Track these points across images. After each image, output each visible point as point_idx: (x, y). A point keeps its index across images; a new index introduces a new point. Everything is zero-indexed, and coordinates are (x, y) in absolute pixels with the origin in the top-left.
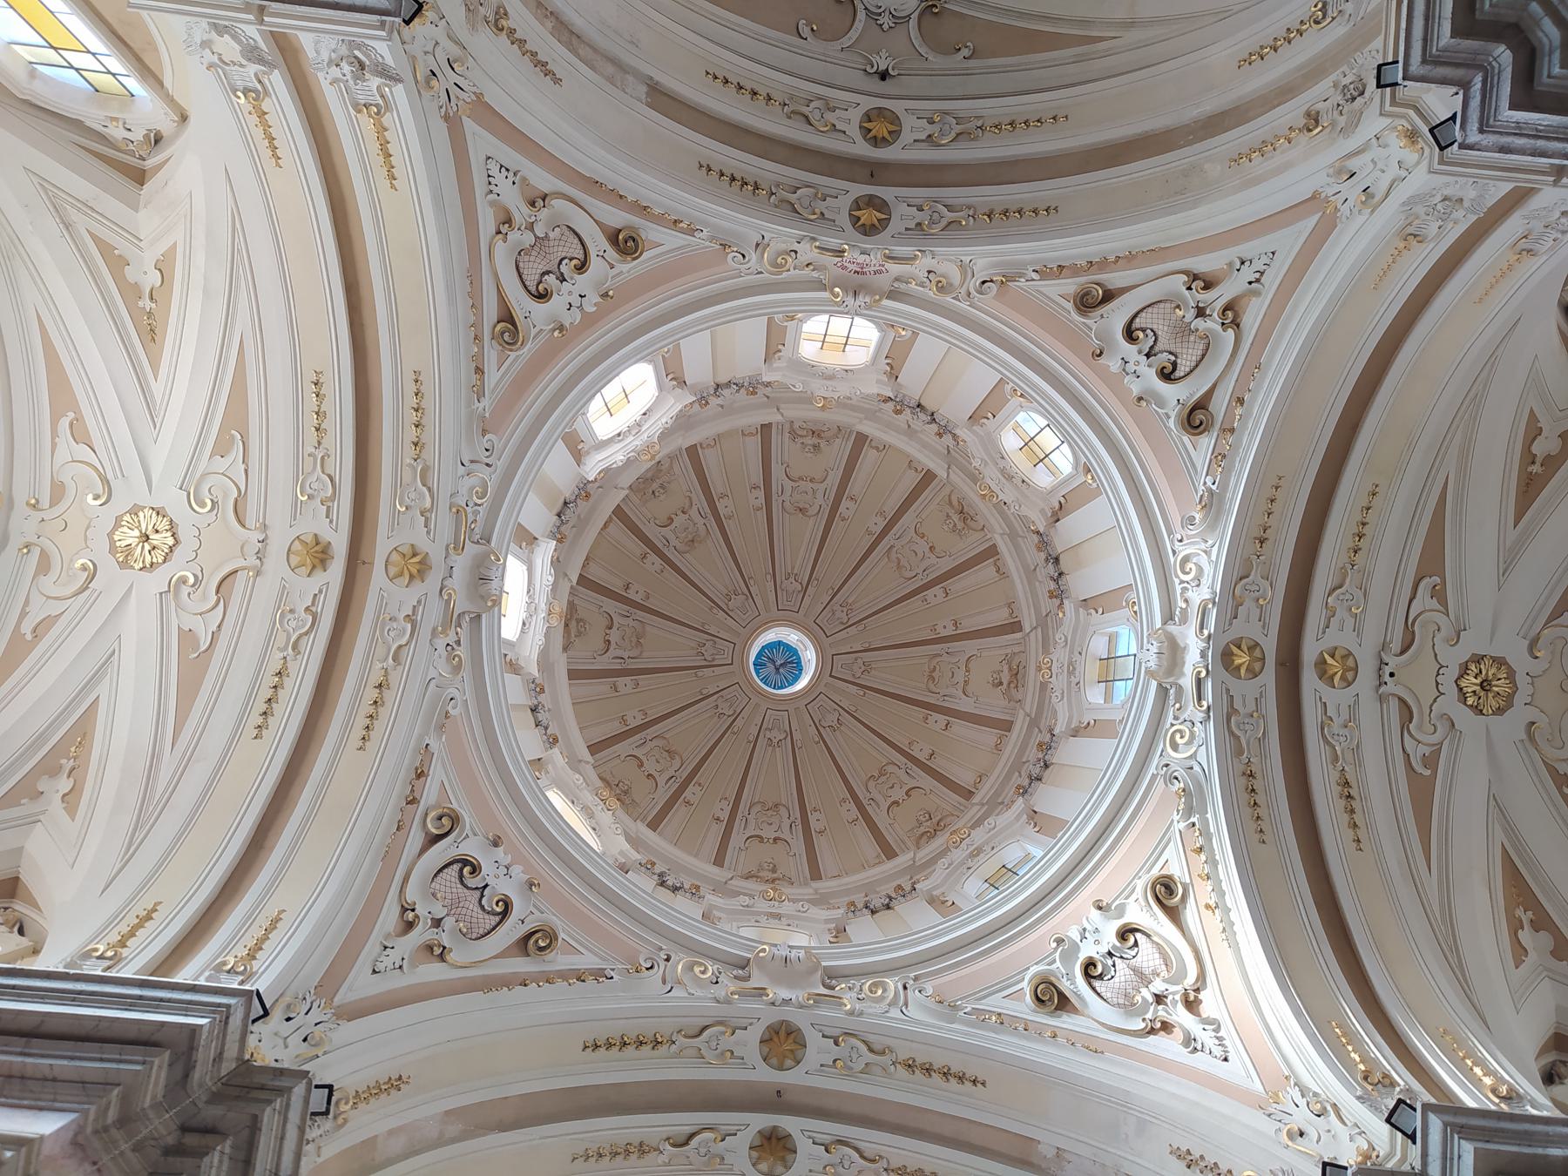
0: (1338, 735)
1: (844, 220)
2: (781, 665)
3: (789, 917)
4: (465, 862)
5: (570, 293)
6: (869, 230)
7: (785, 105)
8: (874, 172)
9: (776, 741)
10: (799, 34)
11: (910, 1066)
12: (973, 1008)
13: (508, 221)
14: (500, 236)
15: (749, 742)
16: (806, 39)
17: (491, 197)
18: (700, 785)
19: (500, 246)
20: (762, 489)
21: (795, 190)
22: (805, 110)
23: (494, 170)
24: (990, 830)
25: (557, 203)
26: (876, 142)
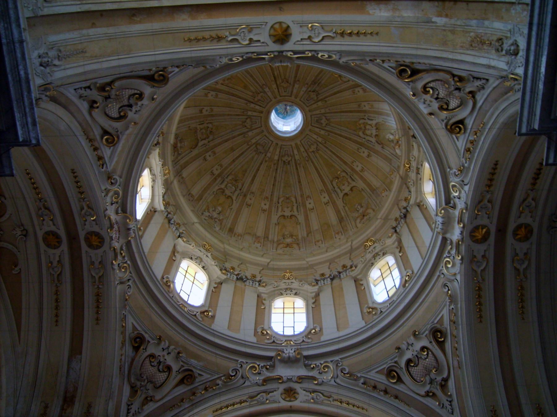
0: (315, 34)
1: (100, 251)
2: (286, 108)
3: (418, 164)
4: (447, 109)
5: (164, 356)
6: (101, 240)
7: (56, 286)
8: (73, 238)
9: (327, 122)
10: (19, 273)
11: (489, 186)
12: (463, 158)
13: (146, 398)
14: (153, 399)
15: (326, 101)
16: (20, 269)
17: (140, 411)
18: (353, 162)
19: (157, 397)
20: (204, 156)
21: (93, 277)
22: (56, 276)
23: (449, 407)
24: (382, 246)
25: (133, 380)
26: (60, 242)
